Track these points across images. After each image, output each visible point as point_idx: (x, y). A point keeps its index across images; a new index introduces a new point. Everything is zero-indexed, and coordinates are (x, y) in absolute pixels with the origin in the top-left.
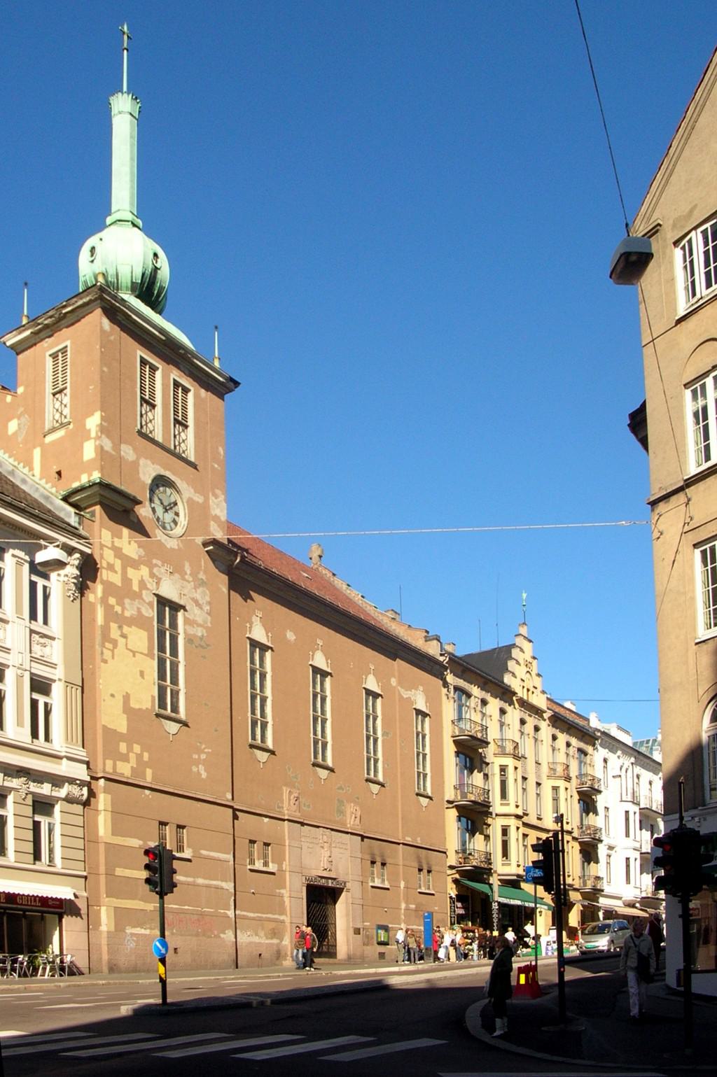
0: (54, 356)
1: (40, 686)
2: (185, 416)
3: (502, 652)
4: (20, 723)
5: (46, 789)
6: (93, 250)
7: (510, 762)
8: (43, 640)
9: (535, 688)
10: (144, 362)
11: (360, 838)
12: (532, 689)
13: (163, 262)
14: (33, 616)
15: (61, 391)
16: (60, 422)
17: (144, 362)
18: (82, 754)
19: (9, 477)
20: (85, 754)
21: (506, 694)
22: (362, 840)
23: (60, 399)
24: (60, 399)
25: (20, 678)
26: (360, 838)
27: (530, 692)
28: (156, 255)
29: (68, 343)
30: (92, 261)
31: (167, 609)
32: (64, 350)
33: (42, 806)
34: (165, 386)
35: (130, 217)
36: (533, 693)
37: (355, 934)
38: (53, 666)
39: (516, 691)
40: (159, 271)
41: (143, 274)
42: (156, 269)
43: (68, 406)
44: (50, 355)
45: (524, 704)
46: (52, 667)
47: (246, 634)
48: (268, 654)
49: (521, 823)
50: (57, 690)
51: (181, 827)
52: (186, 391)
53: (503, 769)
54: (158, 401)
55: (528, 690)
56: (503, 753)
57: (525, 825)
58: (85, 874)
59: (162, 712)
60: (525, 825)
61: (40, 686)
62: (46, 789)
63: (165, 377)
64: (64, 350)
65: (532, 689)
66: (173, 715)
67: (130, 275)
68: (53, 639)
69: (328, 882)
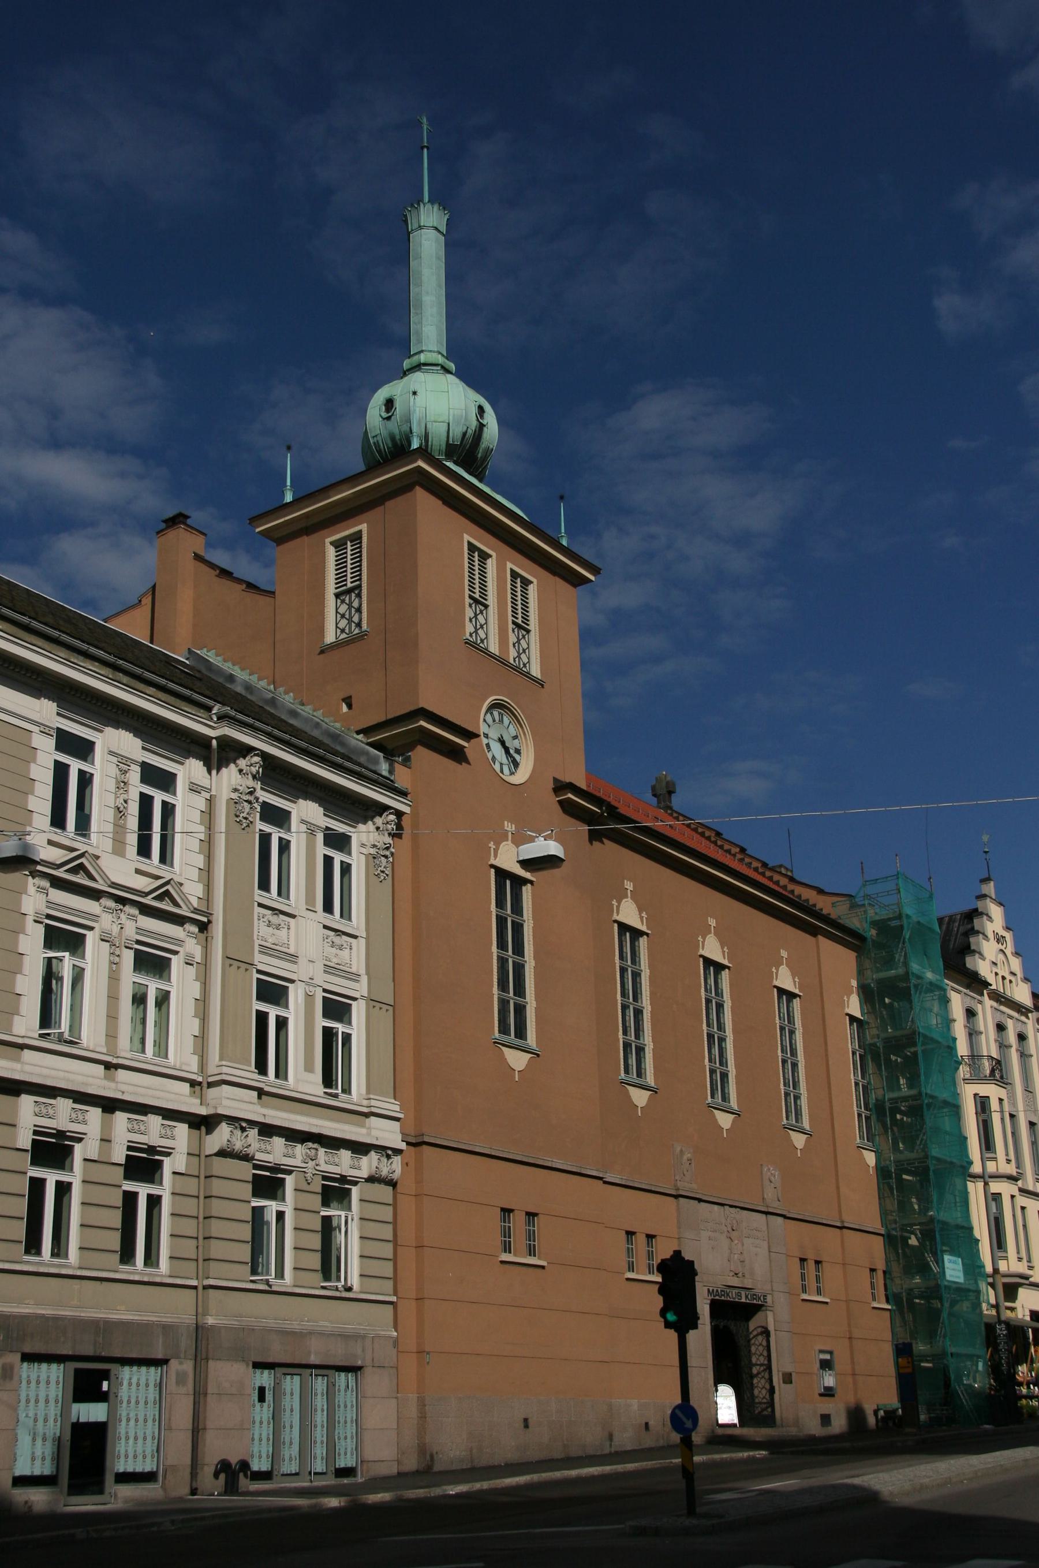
0: (339, 545)
1: (336, 1008)
2: (526, 618)
3: (954, 921)
4: (309, 1068)
5: (344, 1163)
6: (389, 404)
7: (992, 1091)
8: (338, 940)
9: (1013, 974)
10: (472, 548)
11: (256, 1093)
12: (1008, 977)
13: (491, 418)
14: (328, 908)
15: (349, 591)
16: (347, 631)
17: (472, 548)
18: (392, 1107)
19: (268, 708)
20: (397, 1108)
21: (975, 983)
22: (259, 1097)
23: (347, 601)
24: (347, 601)
25: (309, 997)
26: (256, 1093)
27: (1007, 982)
28: (481, 410)
29: (364, 527)
30: (389, 418)
31: (508, 882)
32: (357, 537)
33: (335, 1191)
34: (501, 579)
35: (440, 360)
36: (1011, 982)
37: (784, 1382)
38: (354, 977)
39: (989, 981)
40: (485, 429)
41: (465, 434)
42: (481, 426)
43: (467, 619)
44: (331, 543)
45: (996, 996)
46: (351, 979)
47: (612, 914)
48: (643, 941)
49: (1016, 1188)
50: (358, 1011)
51: (531, 1215)
52: (526, 583)
53: (983, 1104)
54: (492, 600)
55: (1003, 978)
56: (977, 1077)
57: (1023, 1191)
58: (394, 1299)
59: (505, 1038)
60: (1023, 1191)
61: (336, 1008)
62: (344, 1163)
63: (501, 568)
64: (357, 537)
65: (1008, 977)
66: (519, 1042)
67: (445, 434)
68: (355, 937)
69: (739, 1295)
